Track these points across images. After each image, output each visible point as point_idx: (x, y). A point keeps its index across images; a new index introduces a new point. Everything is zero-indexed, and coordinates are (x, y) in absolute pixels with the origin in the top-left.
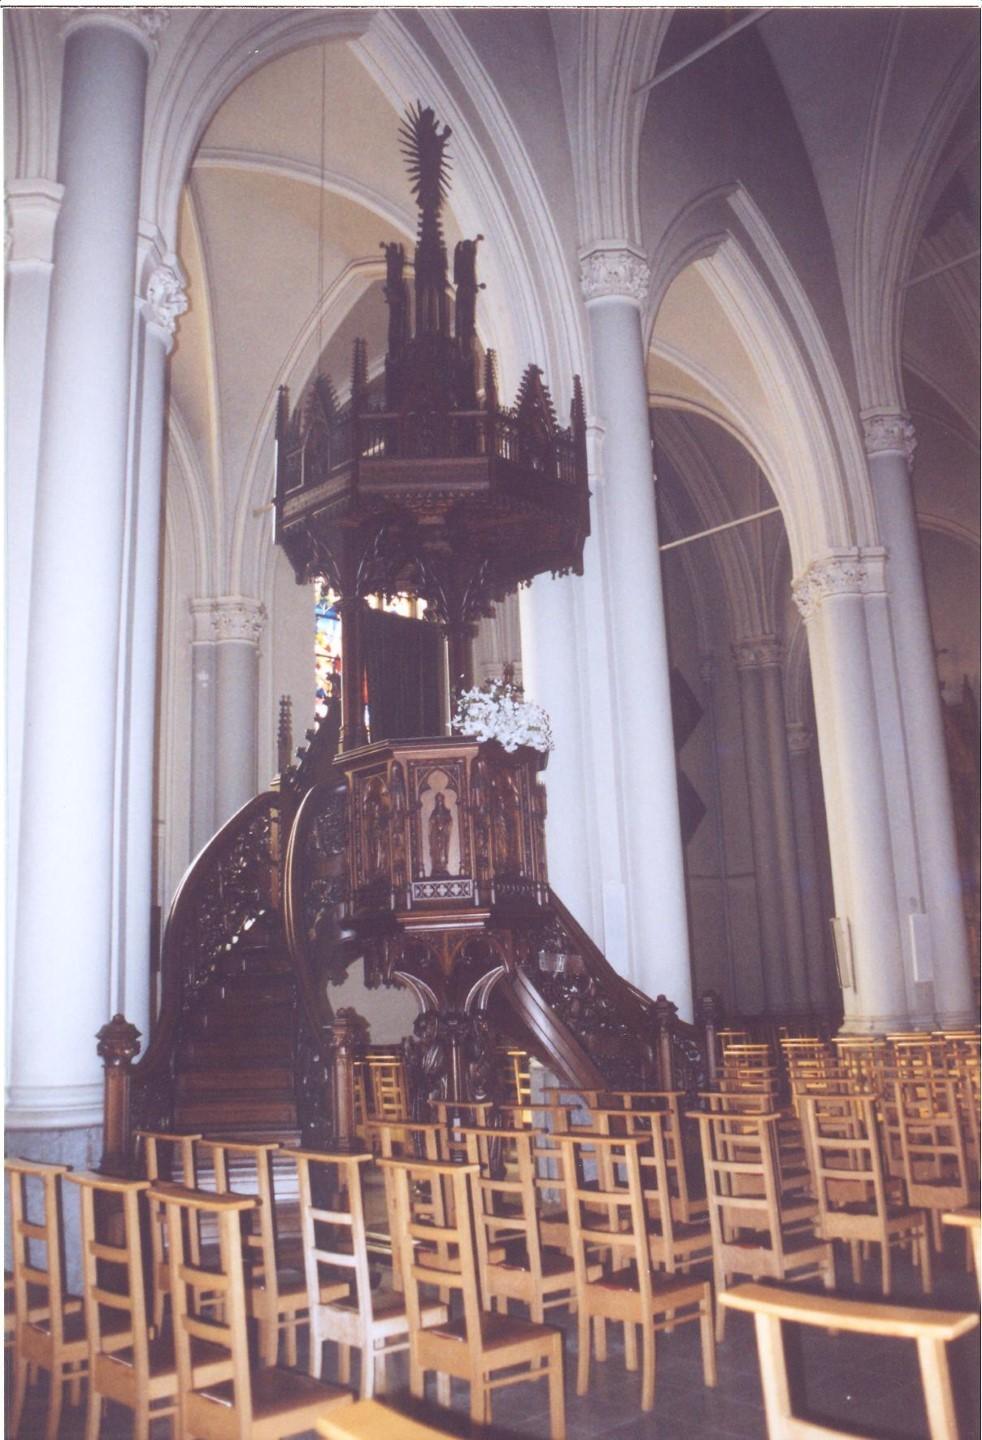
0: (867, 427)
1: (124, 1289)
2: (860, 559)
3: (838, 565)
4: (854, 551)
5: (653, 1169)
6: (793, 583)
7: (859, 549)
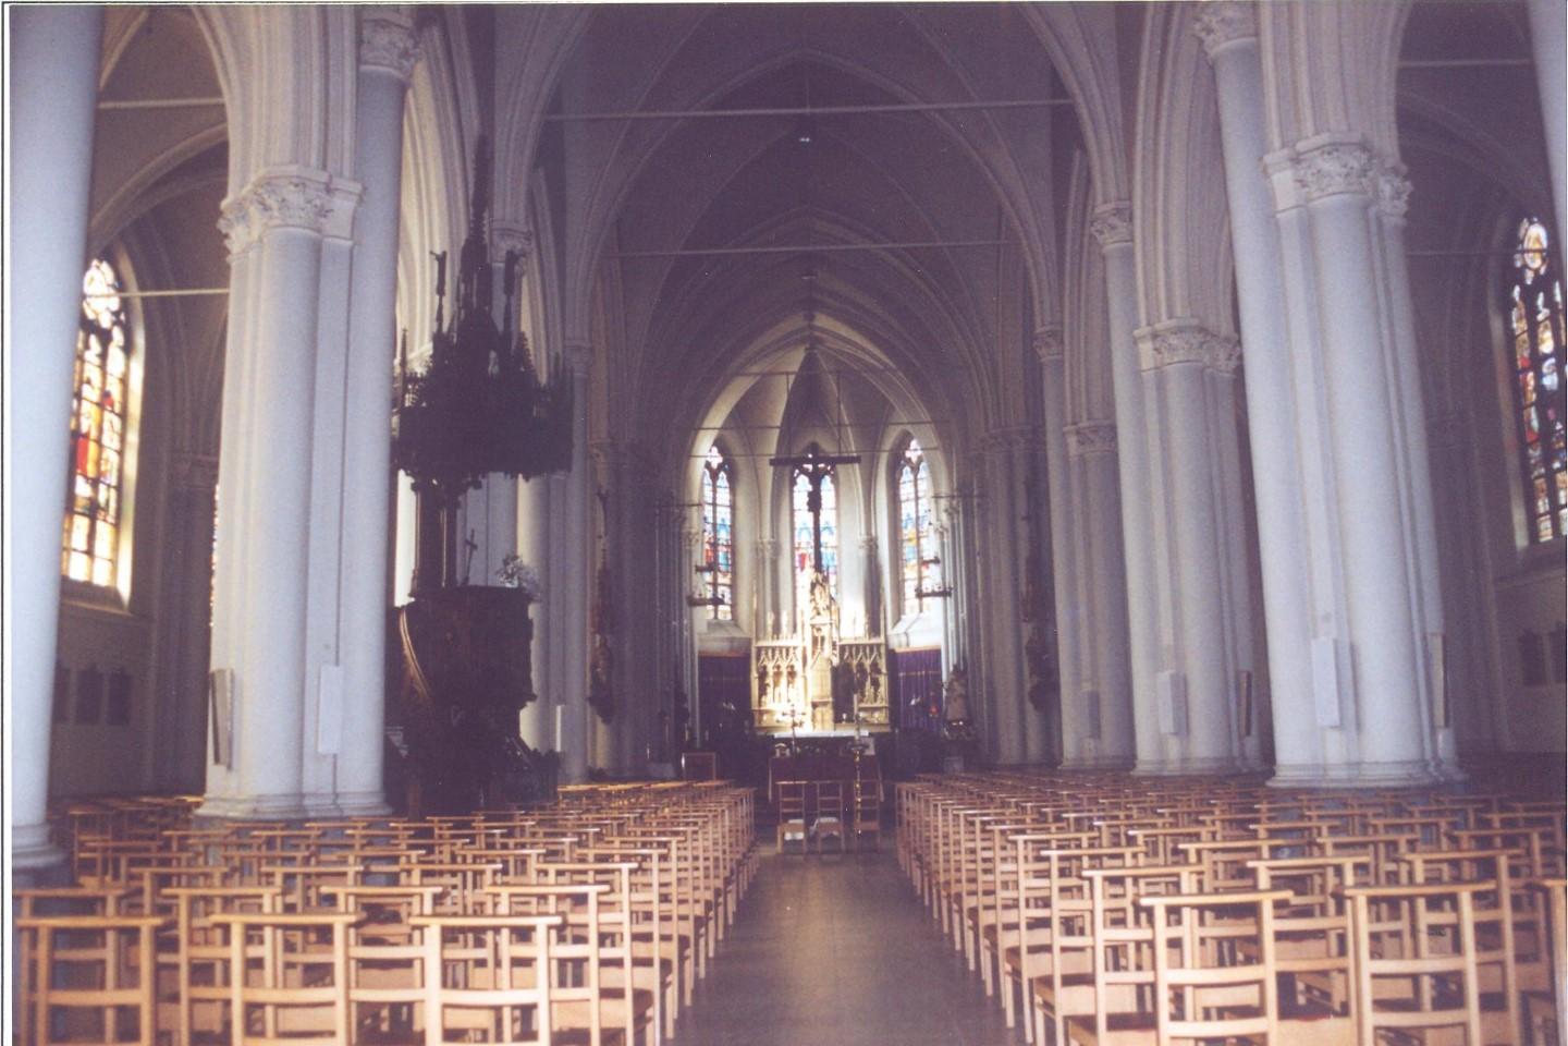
0: (366, 33)
1: (1480, 927)
2: (329, 190)
3: (301, 187)
4: (324, 177)
5: (596, 855)
6: (224, 204)
7: (331, 177)
